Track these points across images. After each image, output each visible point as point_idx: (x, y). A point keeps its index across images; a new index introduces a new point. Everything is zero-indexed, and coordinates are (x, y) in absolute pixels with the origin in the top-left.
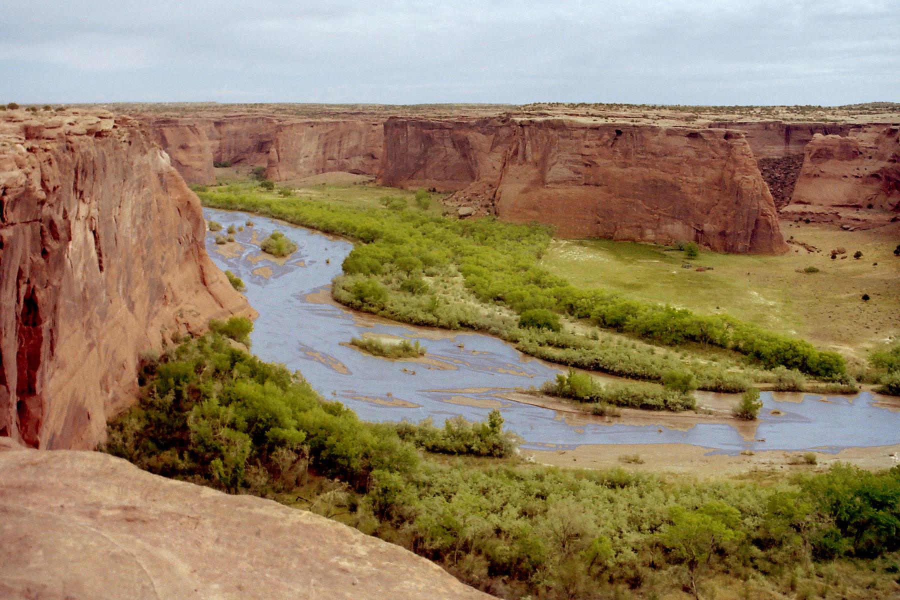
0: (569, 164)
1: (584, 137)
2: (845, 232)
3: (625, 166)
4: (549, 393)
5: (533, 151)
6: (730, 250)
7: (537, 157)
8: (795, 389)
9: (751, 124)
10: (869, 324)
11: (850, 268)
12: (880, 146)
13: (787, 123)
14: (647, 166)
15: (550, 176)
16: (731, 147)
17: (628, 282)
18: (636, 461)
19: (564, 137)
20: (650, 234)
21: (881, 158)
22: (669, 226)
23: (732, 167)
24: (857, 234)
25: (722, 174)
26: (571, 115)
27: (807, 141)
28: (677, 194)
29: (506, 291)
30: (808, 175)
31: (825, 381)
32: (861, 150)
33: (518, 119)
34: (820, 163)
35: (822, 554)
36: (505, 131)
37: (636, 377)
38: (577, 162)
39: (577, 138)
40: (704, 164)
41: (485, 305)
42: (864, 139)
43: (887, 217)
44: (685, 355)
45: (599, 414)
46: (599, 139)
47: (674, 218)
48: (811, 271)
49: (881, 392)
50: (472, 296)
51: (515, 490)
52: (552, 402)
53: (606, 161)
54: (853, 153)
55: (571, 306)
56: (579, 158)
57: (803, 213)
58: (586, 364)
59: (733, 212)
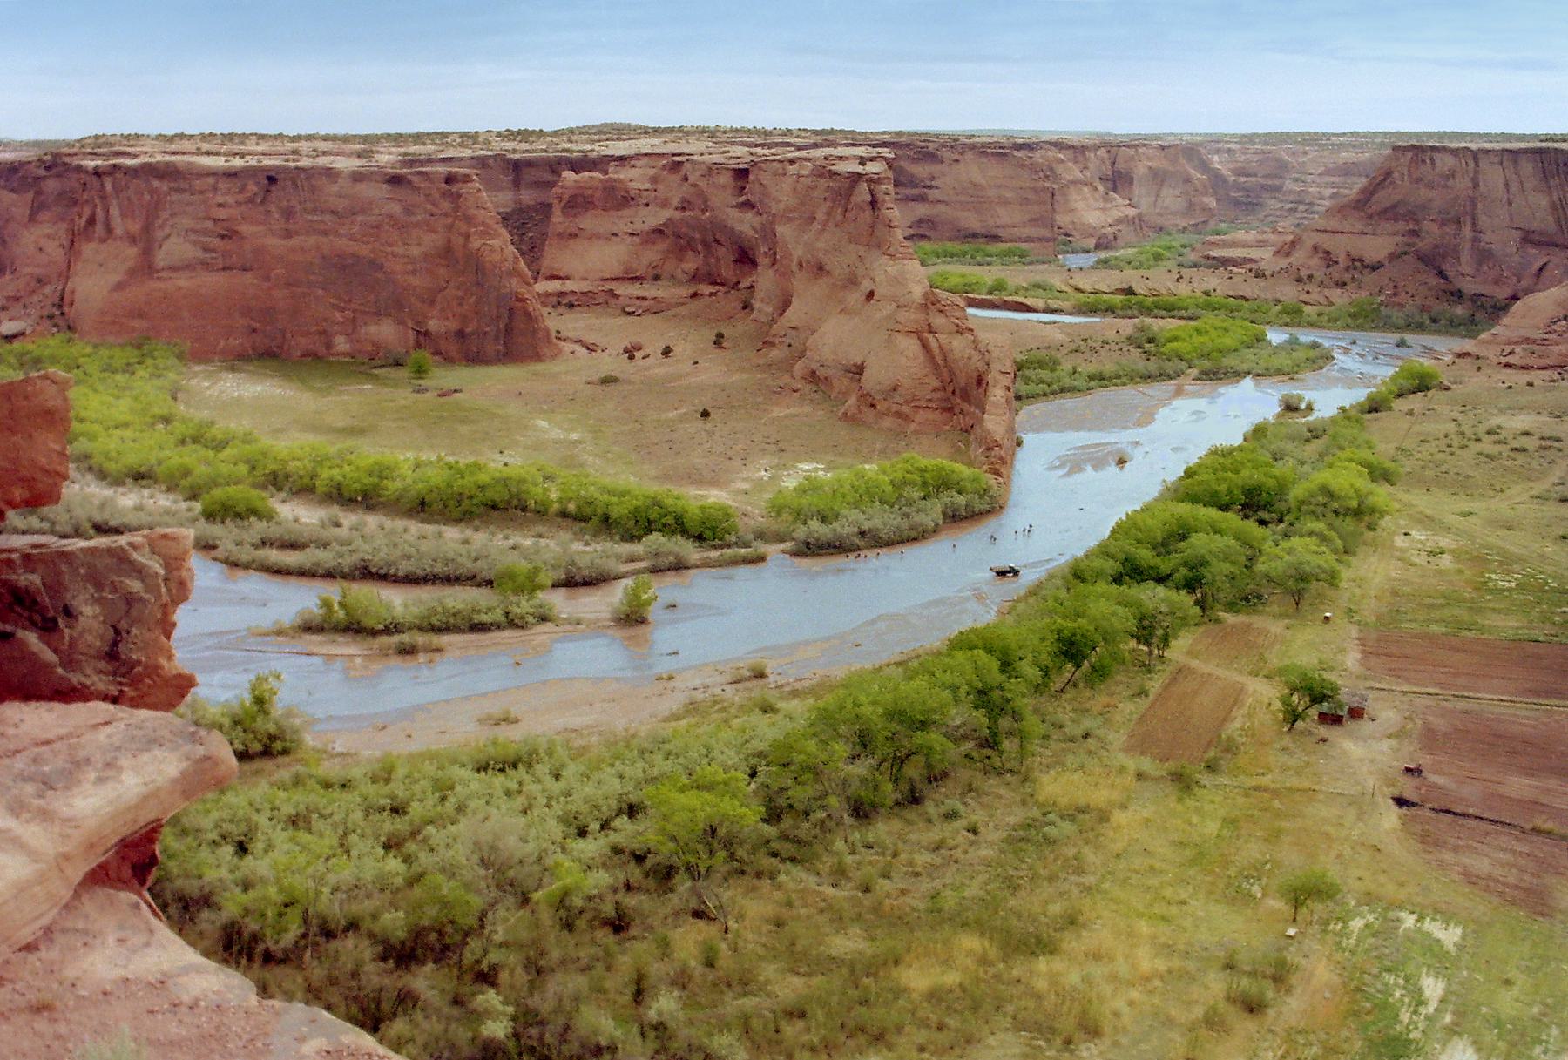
0: (193, 237)
1: (215, 189)
2: (631, 318)
3: (288, 234)
4: (309, 628)
5: (123, 215)
6: (475, 359)
7: (135, 227)
8: (679, 566)
9: (461, 159)
10: (730, 453)
11: (660, 371)
12: (660, 187)
13: (517, 156)
14: (325, 233)
15: (161, 258)
16: (459, 196)
17: (340, 425)
18: (507, 720)
19: (179, 190)
20: (341, 344)
21: (665, 204)
22: (372, 329)
23: (463, 227)
24: (648, 319)
25: (449, 241)
26: (174, 153)
27: (553, 184)
28: (379, 275)
29: (153, 462)
30: (560, 235)
31: (715, 547)
32: (632, 194)
33: (91, 164)
34: (575, 216)
35: (862, 811)
36: (51, 185)
37: (449, 580)
38: (205, 232)
39: (202, 192)
40: (417, 225)
41: (121, 490)
42: (634, 178)
43: (685, 291)
44: (493, 534)
45: (408, 651)
46: (240, 192)
47: (378, 314)
48: (608, 381)
49: (796, 554)
50: (89, 477)
51: (345, 806)
52: (321, 643)
53: (255, 229)
54: (620, 199)
55: (274, 474)
56: (209, 224)
57: (562, 294)
58: (346, 570)
59: (472, 300)
